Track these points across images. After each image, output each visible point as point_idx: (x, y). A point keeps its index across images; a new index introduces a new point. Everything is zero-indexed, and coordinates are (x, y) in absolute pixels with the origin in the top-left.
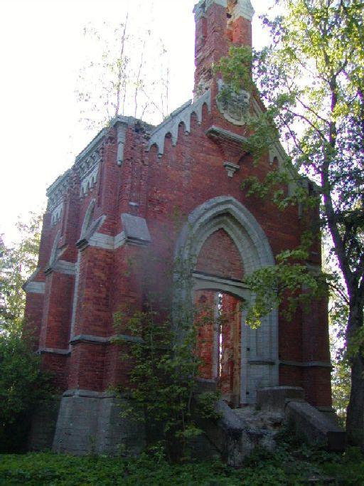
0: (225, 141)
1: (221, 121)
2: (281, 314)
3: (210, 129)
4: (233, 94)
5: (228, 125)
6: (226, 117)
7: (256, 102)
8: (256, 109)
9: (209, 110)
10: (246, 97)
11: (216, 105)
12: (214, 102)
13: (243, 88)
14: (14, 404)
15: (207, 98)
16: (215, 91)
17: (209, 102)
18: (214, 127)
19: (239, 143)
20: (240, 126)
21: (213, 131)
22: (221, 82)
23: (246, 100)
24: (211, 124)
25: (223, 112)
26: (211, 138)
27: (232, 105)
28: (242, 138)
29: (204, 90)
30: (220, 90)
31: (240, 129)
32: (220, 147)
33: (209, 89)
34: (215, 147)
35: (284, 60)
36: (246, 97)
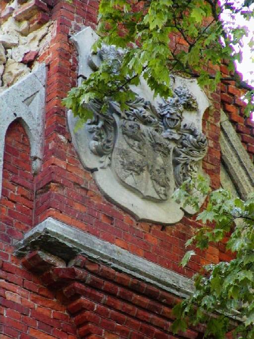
0: (94, 286)
1: (83, 201)
2: (101, 236)
3: (39, 228)
4: (143, 91)
5: (111, 218)
6: (108, 182)
7: (231, 130)
8: (232, 161)
9: (36, 150)
10: (190, 106)
11: (63, 130)
12: (55, 121)
13: (178, 66)
14: (160, 43)
15: (28, 101)
16: (64, 70)
17: (34, 117)
18: (52, 225)
19: (157, 297)
20: (164, 226)
21: (48, 243)
22: (87, 39)
23: (192, 120)
24: (42, 212)
25: (90, 161)
26: (36, 270)
27: (133, 136)
28: (185, 283)
29: (15, 67)
30: (84, 70)
31: (166, 241)
32: (73, 313)
33: (38, 67)
34: (50, 310)
35: (128, 115)
36: (190, 106)
